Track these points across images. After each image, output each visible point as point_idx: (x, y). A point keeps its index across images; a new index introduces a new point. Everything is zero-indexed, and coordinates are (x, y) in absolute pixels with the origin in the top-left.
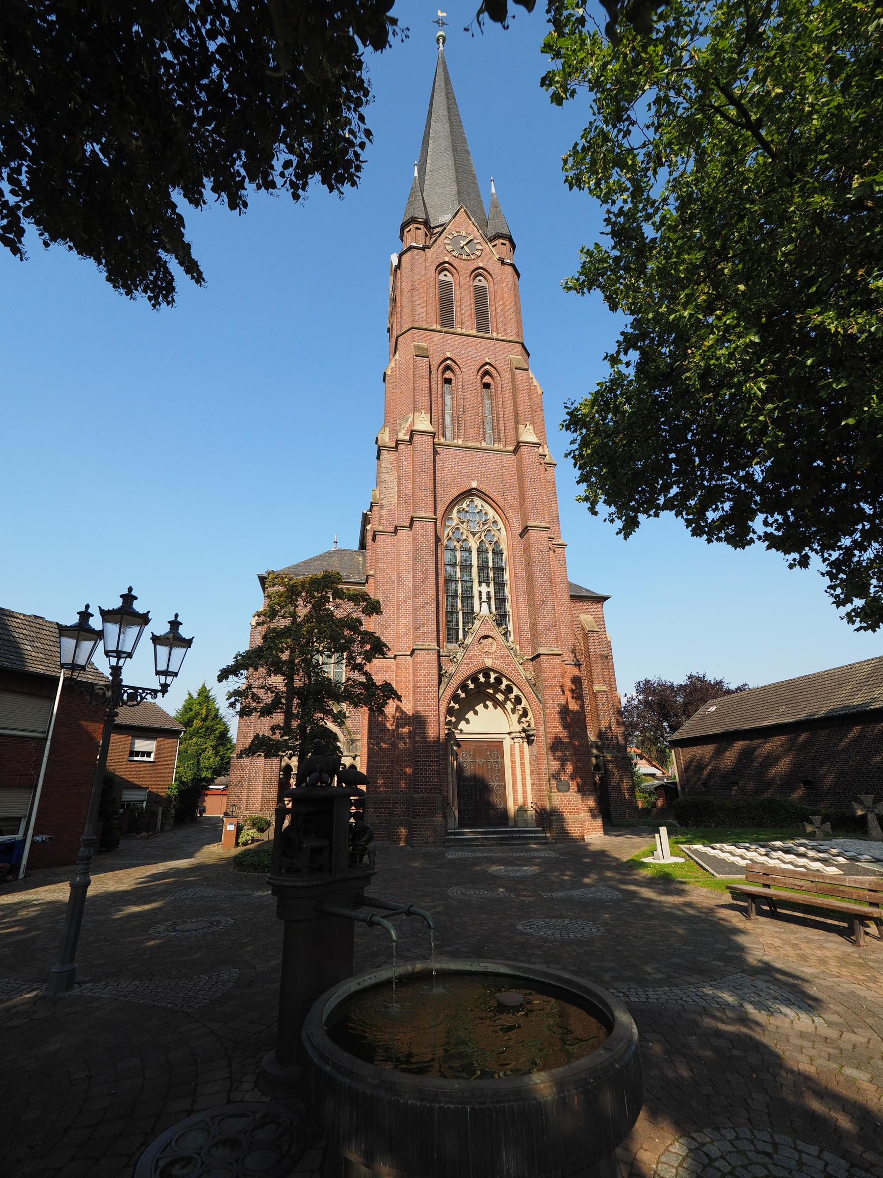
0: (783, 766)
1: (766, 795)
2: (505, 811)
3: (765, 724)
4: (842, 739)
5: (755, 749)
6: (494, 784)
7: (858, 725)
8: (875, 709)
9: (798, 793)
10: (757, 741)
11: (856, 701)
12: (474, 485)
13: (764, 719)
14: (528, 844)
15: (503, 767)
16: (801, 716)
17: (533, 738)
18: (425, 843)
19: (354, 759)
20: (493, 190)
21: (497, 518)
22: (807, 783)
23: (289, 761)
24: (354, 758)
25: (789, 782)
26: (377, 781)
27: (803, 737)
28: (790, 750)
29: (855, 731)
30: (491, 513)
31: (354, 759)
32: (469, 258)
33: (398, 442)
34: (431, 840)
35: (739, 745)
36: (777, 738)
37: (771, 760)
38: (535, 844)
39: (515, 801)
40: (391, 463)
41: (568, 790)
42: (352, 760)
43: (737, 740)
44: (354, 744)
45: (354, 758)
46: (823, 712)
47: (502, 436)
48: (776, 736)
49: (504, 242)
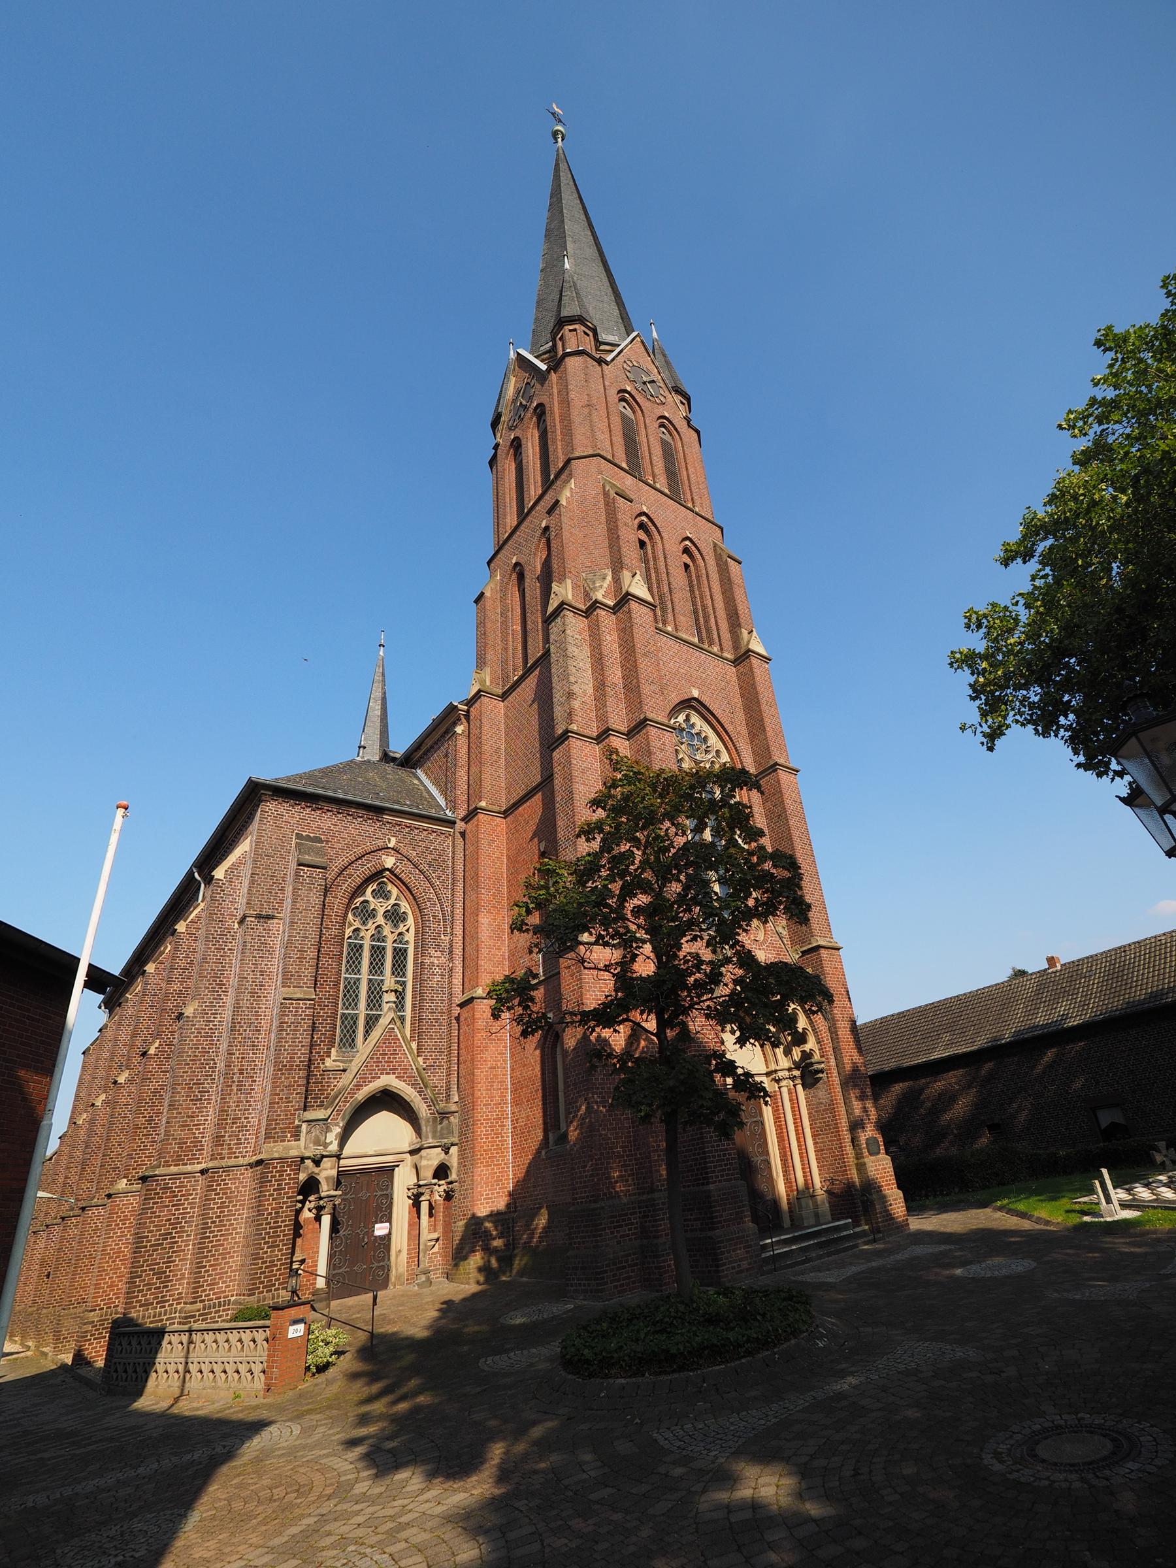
0: (961, 1108)
1: (939, 1152)
2: (776, 1202)
3: (935, 1056)
4: (1034, 1067)
5: (921, 1091)
6: (758, 1160)
7: (1053, 1047)
8: (1074, 1027)
9: (985, 1140)
10: (924, 1081)
11: (1041, 1019)
12: (696, 694)
13: (916, 1054)
14: (856, 1246)
15: (764, 1129)
16: (980, 1042)
17: (821, 1075)
18: (738, 1273)
19: (447, 1153)
20: (655, 335)
21: (720, 746)
22: (993, 1128)
23: (316, 1170)
24: (446, 1150)
25: (969, 1128)
26: (609, 1173)
27: (988, 1067)
28: (969, 1087)
29: (1050, 1054)
30: (713, 739)
31: (447, 1153)
32: (651, 398)
33: (595, 605)
34: (745, 1264)
35: (898, 1088)
36: (951, 1074)
37: (947, 1099)
38: (866, 1243)
39: (787, 1182)
40: (580, 633)
41: (878, 1153)
42: (443, 1155)
43: (896, 1082)
44: (445, 1122)
45: (446, 1150)
46: (1007, 1037)
47: (715, 636)
48: (949, 1071)
49: (684, 401)
